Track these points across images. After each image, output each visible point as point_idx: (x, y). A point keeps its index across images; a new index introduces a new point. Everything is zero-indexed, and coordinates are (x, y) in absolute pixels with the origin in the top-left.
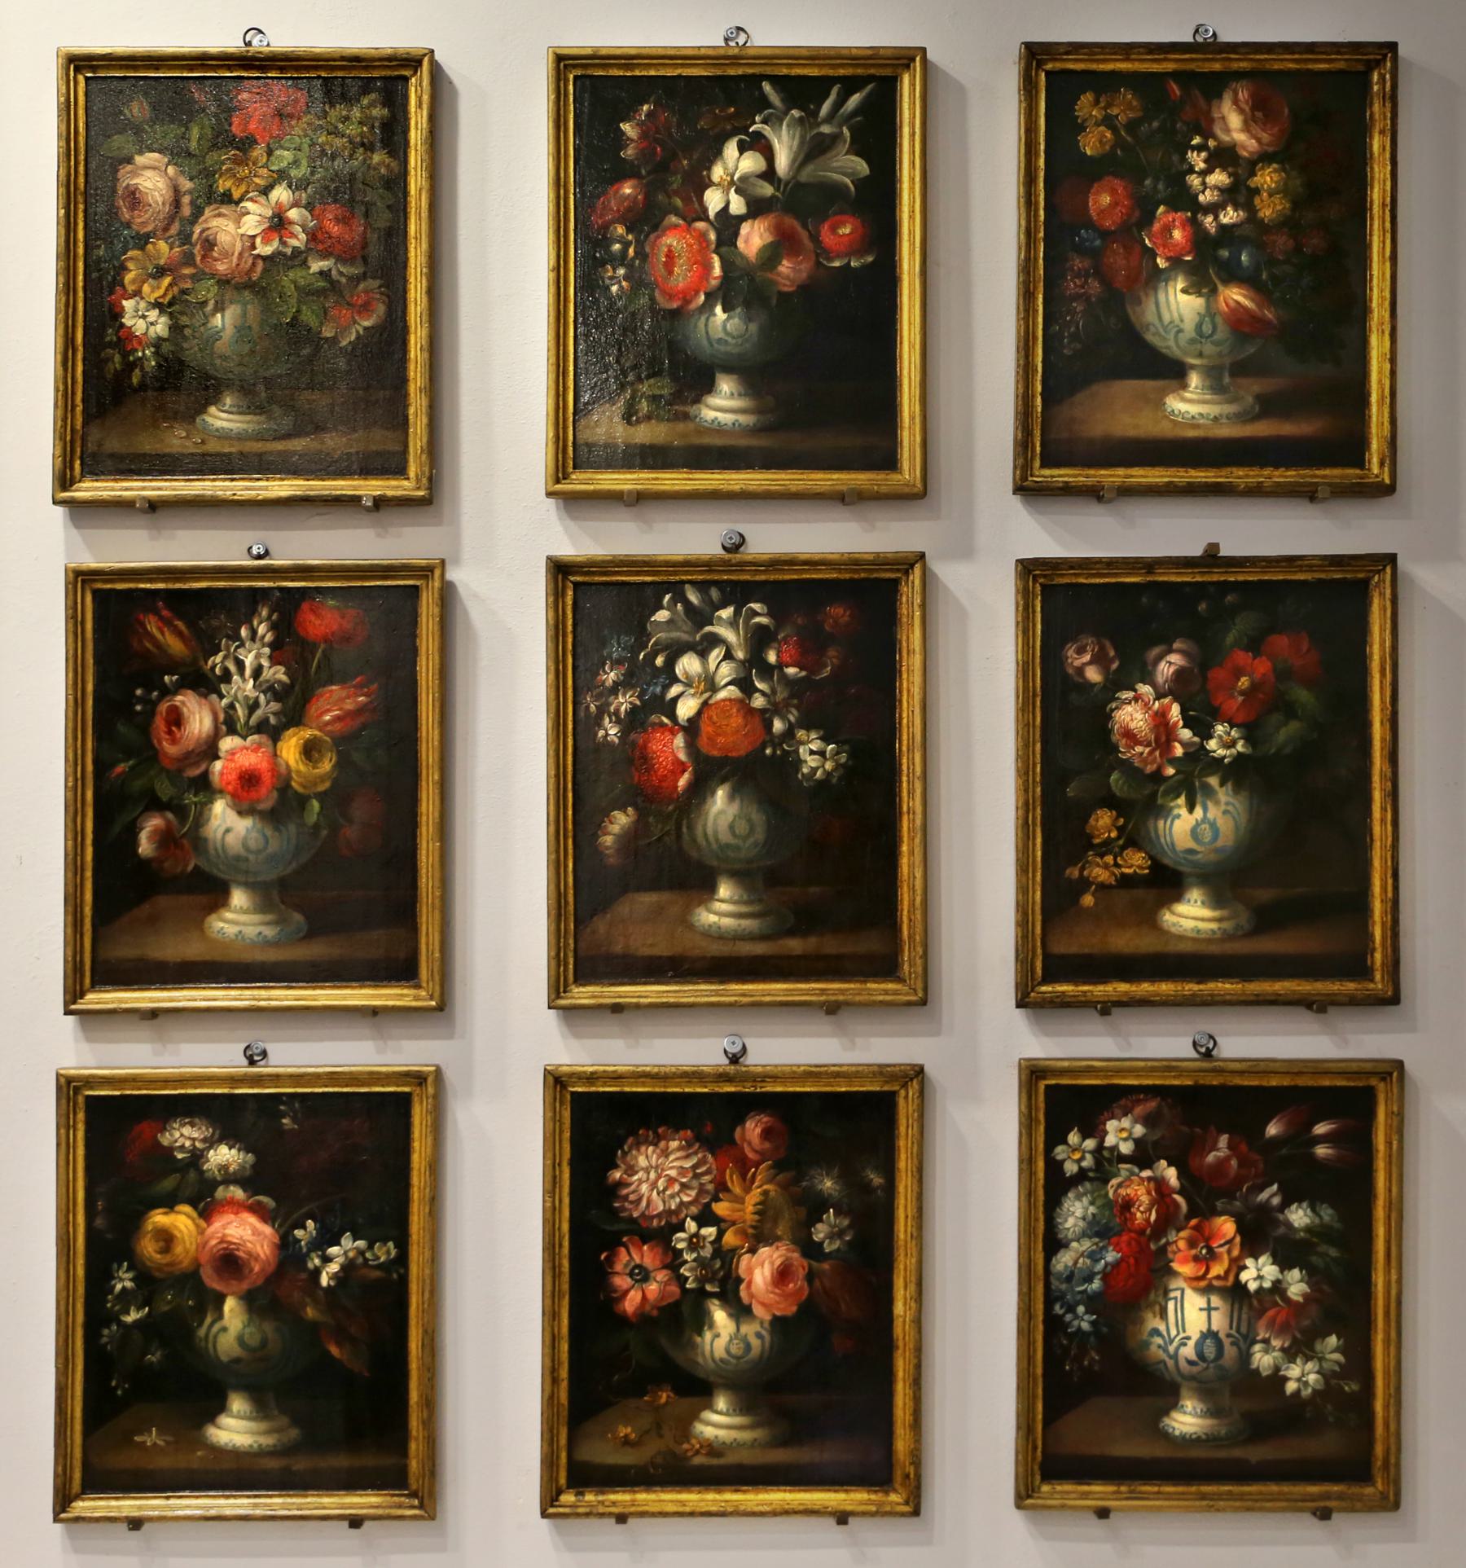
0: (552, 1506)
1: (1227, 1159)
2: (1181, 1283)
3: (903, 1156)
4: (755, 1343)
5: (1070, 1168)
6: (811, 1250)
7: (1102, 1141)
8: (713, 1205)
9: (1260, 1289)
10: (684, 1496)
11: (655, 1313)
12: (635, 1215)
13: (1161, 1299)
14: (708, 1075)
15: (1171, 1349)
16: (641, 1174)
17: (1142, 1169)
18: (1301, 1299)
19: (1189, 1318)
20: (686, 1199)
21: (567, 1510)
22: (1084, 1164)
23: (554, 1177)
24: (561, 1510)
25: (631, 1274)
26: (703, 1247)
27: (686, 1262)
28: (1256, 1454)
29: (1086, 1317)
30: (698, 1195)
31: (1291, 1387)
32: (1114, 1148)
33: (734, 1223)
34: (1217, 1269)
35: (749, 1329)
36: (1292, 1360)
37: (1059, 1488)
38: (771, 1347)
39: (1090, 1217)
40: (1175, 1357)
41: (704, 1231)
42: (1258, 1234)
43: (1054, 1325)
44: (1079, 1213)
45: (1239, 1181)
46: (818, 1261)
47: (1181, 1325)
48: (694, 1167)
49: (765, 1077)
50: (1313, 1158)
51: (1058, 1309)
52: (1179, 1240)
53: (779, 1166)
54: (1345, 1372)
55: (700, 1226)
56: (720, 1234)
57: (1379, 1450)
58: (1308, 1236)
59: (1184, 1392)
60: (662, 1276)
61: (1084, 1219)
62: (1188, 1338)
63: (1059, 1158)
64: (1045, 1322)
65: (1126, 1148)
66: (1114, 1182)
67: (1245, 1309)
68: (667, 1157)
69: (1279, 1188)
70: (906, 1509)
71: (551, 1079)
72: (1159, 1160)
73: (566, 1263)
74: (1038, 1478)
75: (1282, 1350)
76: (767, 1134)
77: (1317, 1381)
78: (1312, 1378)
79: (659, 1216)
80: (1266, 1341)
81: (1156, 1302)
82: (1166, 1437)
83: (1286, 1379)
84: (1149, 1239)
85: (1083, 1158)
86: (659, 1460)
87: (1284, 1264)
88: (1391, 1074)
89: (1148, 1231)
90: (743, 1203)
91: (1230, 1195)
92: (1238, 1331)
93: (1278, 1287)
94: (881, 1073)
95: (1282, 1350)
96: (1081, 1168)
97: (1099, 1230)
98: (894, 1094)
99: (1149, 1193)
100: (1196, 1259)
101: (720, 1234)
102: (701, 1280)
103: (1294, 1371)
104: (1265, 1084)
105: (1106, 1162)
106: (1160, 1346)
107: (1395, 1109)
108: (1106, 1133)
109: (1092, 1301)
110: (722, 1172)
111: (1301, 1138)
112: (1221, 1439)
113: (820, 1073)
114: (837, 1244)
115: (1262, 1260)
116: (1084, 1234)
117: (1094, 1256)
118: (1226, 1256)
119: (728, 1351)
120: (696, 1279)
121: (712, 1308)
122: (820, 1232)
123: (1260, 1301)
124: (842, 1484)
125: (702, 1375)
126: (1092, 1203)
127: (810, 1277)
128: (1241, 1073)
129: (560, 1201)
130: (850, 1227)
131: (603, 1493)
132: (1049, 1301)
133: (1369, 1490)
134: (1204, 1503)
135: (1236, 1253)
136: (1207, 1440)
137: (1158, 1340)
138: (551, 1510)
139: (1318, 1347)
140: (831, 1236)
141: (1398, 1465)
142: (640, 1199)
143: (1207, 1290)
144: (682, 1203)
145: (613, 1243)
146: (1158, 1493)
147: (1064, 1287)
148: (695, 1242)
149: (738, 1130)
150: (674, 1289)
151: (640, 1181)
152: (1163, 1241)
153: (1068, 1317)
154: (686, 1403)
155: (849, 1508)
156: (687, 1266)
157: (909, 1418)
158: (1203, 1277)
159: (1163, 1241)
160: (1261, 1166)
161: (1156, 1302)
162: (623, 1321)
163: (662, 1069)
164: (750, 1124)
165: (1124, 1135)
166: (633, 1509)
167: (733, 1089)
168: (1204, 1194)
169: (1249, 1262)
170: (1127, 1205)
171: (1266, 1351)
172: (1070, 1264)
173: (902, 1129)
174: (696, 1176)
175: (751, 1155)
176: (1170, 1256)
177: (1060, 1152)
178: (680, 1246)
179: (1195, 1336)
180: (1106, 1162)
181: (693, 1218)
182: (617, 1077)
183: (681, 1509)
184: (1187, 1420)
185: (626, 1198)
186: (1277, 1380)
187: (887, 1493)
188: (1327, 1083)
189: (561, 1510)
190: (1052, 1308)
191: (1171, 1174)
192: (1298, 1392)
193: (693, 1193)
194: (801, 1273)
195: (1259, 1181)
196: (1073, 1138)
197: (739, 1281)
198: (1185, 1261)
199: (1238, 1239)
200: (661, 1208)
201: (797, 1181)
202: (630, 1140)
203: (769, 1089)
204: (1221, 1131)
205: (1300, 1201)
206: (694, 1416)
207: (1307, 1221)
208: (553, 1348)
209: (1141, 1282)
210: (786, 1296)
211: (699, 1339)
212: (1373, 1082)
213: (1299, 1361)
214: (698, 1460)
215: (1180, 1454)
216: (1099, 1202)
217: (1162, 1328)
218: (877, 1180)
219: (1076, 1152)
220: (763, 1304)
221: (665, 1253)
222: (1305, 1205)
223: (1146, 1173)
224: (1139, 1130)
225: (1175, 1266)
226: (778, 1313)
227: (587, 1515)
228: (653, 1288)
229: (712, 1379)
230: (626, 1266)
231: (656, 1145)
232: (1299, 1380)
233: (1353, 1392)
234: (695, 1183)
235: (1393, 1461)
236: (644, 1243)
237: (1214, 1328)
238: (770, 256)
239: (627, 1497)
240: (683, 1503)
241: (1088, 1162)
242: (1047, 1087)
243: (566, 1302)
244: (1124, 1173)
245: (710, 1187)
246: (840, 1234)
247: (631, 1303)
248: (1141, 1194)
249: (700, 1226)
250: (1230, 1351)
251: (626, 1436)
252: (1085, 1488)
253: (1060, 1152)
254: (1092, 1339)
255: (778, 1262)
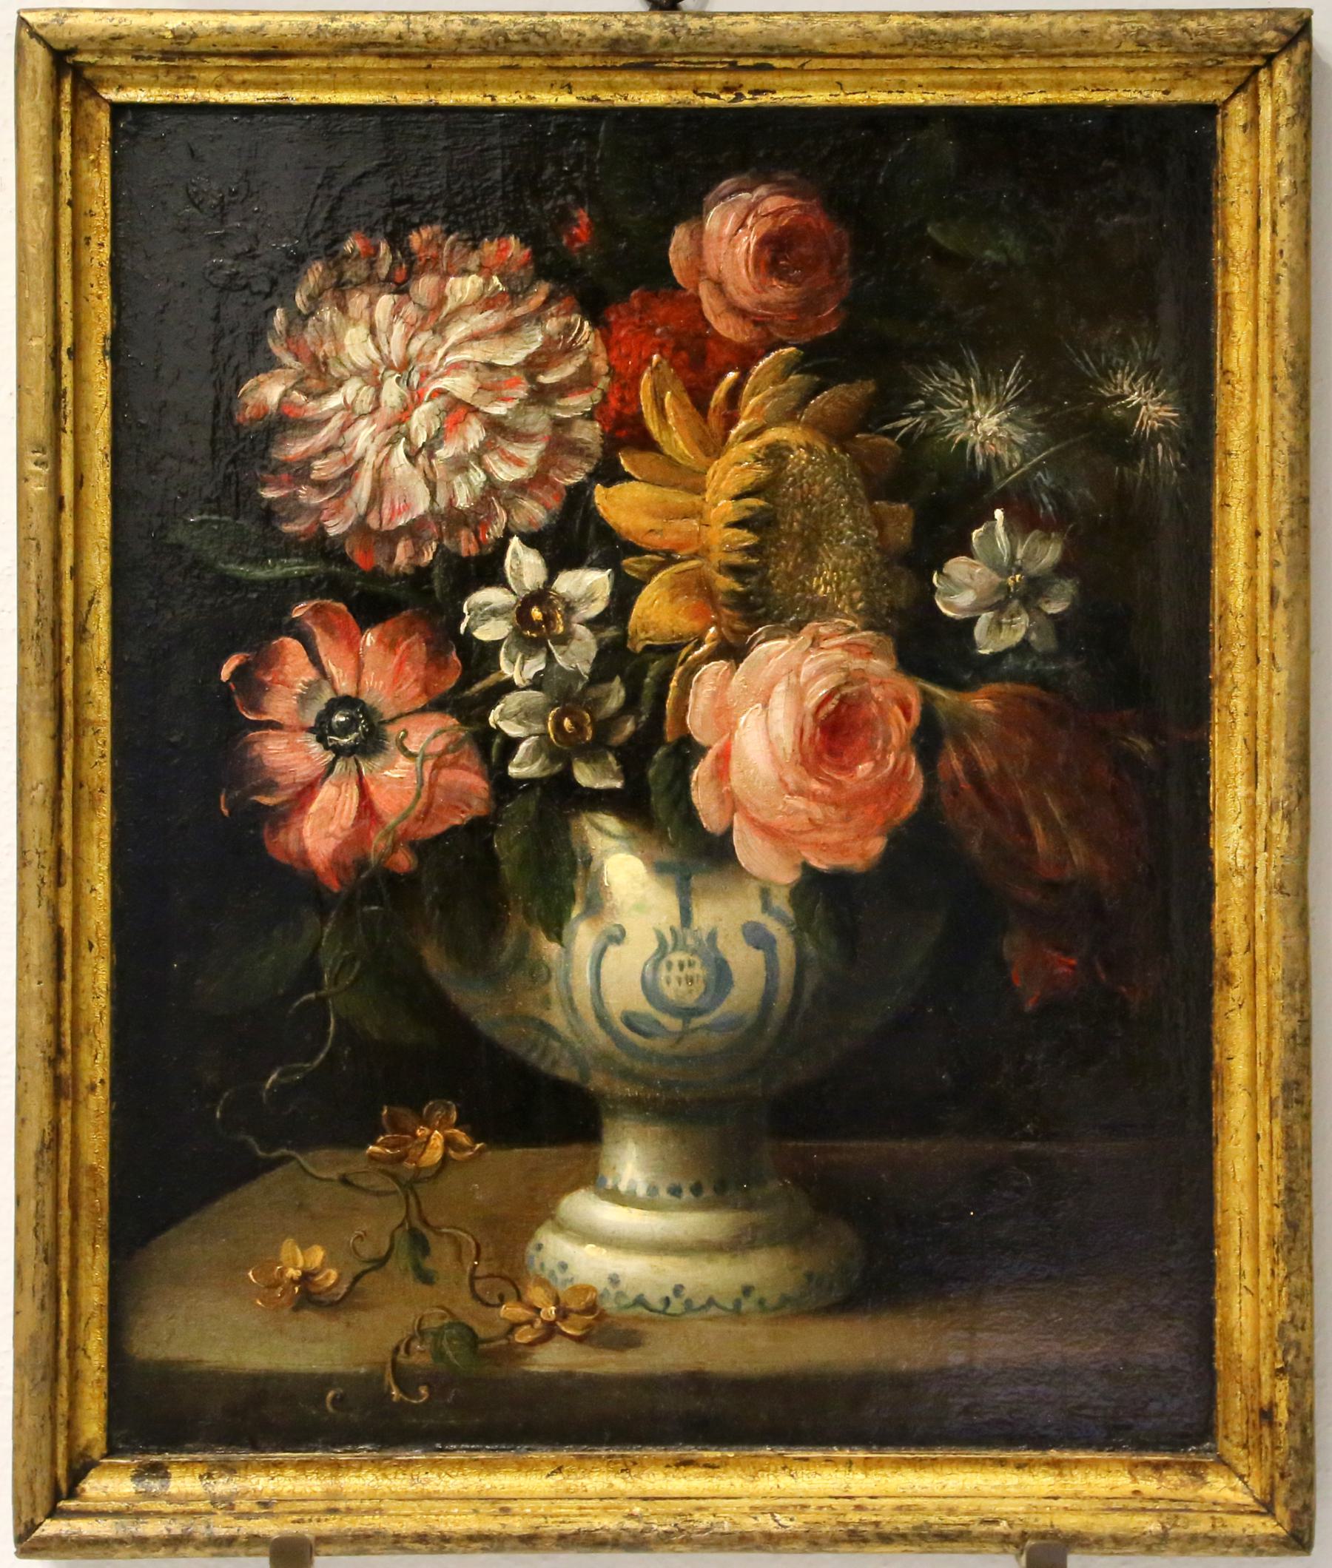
0: (53, 1513)
3: (1241, 328)
4: (746, 964)
6: (929, 645)
8: (600, 493)
10: (506, 1482)
11: (404, 861)
12: (335, 528)
14: (577, 45)
16: (351, 388)
20: (506, 473)
21: (103, 1528)
23: (57, 396)
24: (86, 1527)
25: (322, 730)
26: (564, 640)
27: (509, 686)
30: (546, 462)
33: (669, 558)
35: (723, 914)
38: (801, 963)
41: (568, 583)
46: (959, 686)
48: (532, 366)
49: (769, 54)
53: (822, 362)
55: (554, 568)
56: (625, 593)
60: (428, 734)
68: (439, 331)
70: (1264, 1527)
71: (39, 57)
73: (100, 690)
76: (777, 252)
79: (414, 531)
86: (420, 1357)
90: (699, 490)
94: (1165, 38)
98: (1209, 112)
101: (625, 593)
102: (562, 751)
110: (626, 383)
113: (956, 38)
114: (1018, 629)
119: (650, 990)
120: (544, 745)
121: (598, 843)
122: (961, 587)
124: (1040, 1442)
125: (566, 1072)
127: (929, 738)
129: (79, 482)
130: (1061, 569)
131: (229, 1469)
138: (51, 1528)
140: (1000, 603)
142: (350, 475)
144: (492, 486)
145: (261, 621)
148: (537, 621)
149: (680, 235)
150: (470, 782)
151: (351, 416)
154: (513, 1161)
155: (1069, 1523)
156: (512, 701)
157: (1271, 1218)
162: (296, 887)
163: (419, 25)
164: (719, 220)
166: (329, 1525)
167: (657, 98)
173: (1239, 236)
174: (541, 396)
175: (726, 327)
178: (489, 632)
181: (531, 540)
182: (267, 53)
183: (493, 1525)
185: (301, 471)
187: (1196, 1471)
189: (86, 1527)
193: (531, 454)
194: (899, 728)
197: (687, 751)
200: (421, 505)
201: (876, 413)
202: (315, 274)
203: (784, 97)
206: (537, 1210)
208: (59, 975)
210: (848, 804)
211: (551, 950)
214: (553, 1358)
218: (1151, 408)
220: (769, 831)
221: (436, 658)
226: (822, 863)
227: (174, 1543)
228: (395, 777)
229: (598, 1081)
230: (304, 700)
231: (402, 289)
234: (537, 420)
236: (364, 625)
238: (592, 261)
239: (313, 1484)
240: (503, 1505)
243: (101, 823)
245: (589, 433)
246: (1033, 591)
247: (321, 832)
249: (554, 568)
251: (307, 1277)
255: (818, 691)
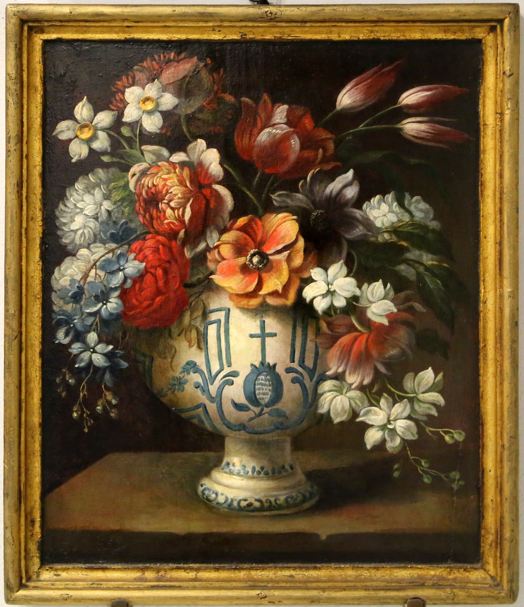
1: (285, 138)
2: (225, 302)
5: (78, 151)
7: (121, 114)
9: (331, 310)
13: (198, 323)
15: (213, 389)
17: (172, 151)
18: (385, 322)
19: (233, 350)
22: (96, 145)
28: (326, 526)
29: (100, 348)
31: (372, 437)
32: (136, 125)
34: (273, 283)
36: (374, 401)
37: (64, 575)
39: (104, 216)
40: (218, 399)
42: (326, 235)
43: (55, 358)
44: (90, 210)
45: (302, 166)
47: (226, 356)
50: (398, 134)
51: (61, 337)
52: (222, 245)
54: (444, 417)
57: (490, 519)
58: (394, 239)
59: (230, 445)
61: (96, 218)
62: (235, 374)
63: (63, 137)
64: (42, 354)
65: (152, 124)
66: (136, 169)
67: (311, 335)
69: (356, 176)
72: (195, 138)
74: (36, 561)
75: (362, 388)
77: (408, 428)
78: (401, 425)
80: (339, 377)
81: (191, 326)
82: (207, 504)
83: (365, 427)
84: (184, 243)
85: (94, 138)
87: (363, 274)
88: (501, 21)
89: (182, 233)
91: (291, 186)
92: (302, 363)
93: (354, 306)
95: (362, 388)
96: (91, 150)
97: (119, 234)
99: (182, 183)
100: (245, 269)
103: (376, 416)
104: (334, 37)
105: (125, 141)
106: (197, 386)
107: (507, 68)
108: (125, 104)
109: (107, 327)
111: (384, 109)
112: (280, 507)
115: (334, 269)
116: (96, 239)
117: (109, 268)
118: (285, 266)
123: (329, 324)
126: (107, 197)
128: (303, 21)
132: (49, 326)
133: (476, 575)
134: (254, 593)
135: (298, 261)
136: (261, 509)
137: (196, 378)
139: (408, 383)
141: (514, 541)
143: (262, 310)
146: (195, 580)
147: (69, 307)
152: (202, 246)
153: (76, 348)
158: (253, 294)
159: (202, 246)
160: (331, 146)
161: (191, 326)
165: (150, 106)
168: (254, 183)
169: (316, 273)
170: (154, 199)
171: (340, 391)
172: (78, 277)
176: (211, 265)
177: (64, 129)
179: (244, 371)
180: (125, 141)
184: (234, 481)
186: (355, 427)
188: (417, 35)
190: (54, 337)
191: (212, 159)
192: (381, 446)
195: (328, 167)
196: (82, 110)
198: (229, 272)
199: (301, 243)
204: (276, 101)
205: (384, 193)
207: (393, 218)
209: (172, 298)
212: (479, 33)
213: (383, 402)
215: (225, 528)
216: (117, 196)
217: (200, 360)
219: (85, 129)
222: (390, 197)
223: (179, 157)
224: (169, 101)
225: (217, 278)
232: (383, 427)
233: (457, 443)
235: (507, 534)
237: (270, 360)
241: (102, 143)
242: (46, 42)
244: (149, 157)
248: (172, 185)
250: (291, 391)
252: (99, 574)
253: (64, 129)
254: (107, 376)
